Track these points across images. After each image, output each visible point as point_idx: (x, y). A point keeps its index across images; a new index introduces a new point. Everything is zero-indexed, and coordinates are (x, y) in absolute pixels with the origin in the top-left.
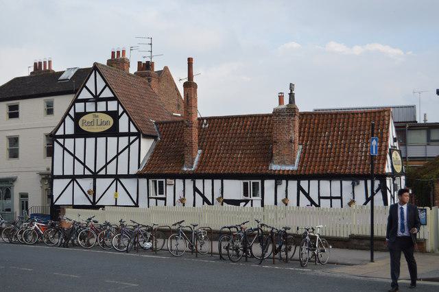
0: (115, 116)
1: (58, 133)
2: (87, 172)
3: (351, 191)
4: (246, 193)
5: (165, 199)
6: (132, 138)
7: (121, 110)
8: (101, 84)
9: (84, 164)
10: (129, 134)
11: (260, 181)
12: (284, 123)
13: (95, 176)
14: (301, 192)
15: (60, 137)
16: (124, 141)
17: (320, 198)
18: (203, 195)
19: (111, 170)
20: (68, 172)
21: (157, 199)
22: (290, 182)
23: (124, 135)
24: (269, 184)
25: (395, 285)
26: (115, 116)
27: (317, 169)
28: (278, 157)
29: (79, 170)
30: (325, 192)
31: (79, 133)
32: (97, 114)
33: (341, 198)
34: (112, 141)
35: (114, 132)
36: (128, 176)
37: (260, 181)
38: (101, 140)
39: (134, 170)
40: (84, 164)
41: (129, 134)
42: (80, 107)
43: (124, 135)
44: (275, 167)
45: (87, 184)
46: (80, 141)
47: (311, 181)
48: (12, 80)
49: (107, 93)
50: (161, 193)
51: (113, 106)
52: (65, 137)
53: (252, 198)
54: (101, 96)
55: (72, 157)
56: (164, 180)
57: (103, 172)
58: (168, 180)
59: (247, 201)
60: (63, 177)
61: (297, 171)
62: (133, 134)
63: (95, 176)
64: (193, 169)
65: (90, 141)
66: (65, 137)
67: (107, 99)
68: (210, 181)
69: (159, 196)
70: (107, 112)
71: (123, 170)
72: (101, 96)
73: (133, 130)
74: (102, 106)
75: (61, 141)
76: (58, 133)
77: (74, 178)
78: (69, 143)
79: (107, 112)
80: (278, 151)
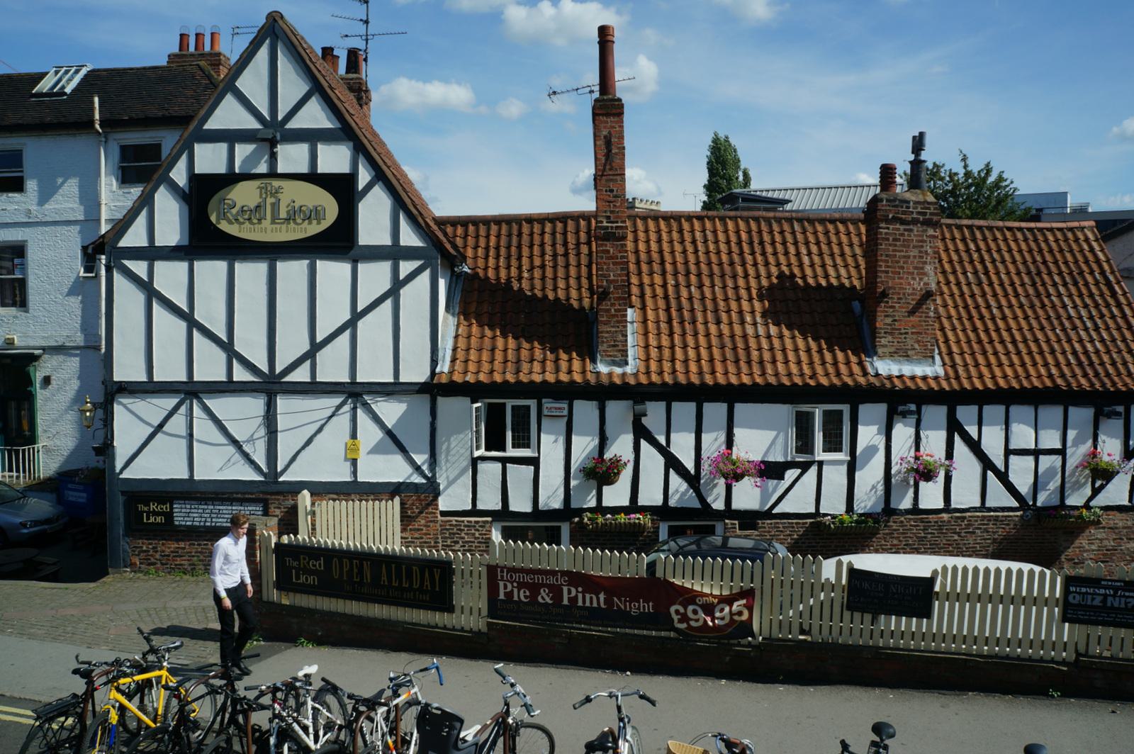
0: (343, 188)
1: (126, 241)
2: (240, 374)
3: (319, 436)
4: (805, 444)
5: (534, 462)
6: (406, 267)
7: (364, 176)
8: (292, 86)
9: (227, 347)
10: (394, 253)
11: (845, 408)
12: (906, 244)
13: (271, 386)
14: (957, 438)
15: (136, 253)
16: (376, 277)
17: (1008, 452)
18: (664, 451)
19: (332, 367)
20: (170, 369)
21: (504, 461)
22: (676, 406)
23: (375, 254)
24: (873, 413)
25: (244, 752)
26: (343, 188)
27: (1005, 377)
28: (890, 338)
29: (210, 366)
30: (1023, 436)
31: (205, 241)
32: (276, 183)
33: (1062, 452)
34: (333, 273)
35: (339, 241)
36: (392, 390)
37: (845, 408)
38: (292, 271)
39: (414, 371)
40: (227, 347)
41: (394, 253)
42: (210, 159)
43: (375, 254)
44: (885, 367)
45: (242, 413)
46: (211, 272)
47: (1072, 410)
48: (125, 70)
49: (315, 116)
50: (522, 442)
51: (335, 159)
52: (152, 253)
53: (820, 455)
54: (292, 125)
55: (183, 325)
56: (532, 403)
57: (301, 375)
58: (548, 404)
59: (805, 467)
60: (150, 388)
61: (636, 375)
62: (410, 253)
63: (271, 386)
64: (629, 369)
65: (251, 274)
66: (152, 253)
67: (312, 137)
68: (663, 405)
69: (511, 452)
70: (313, 177)
71: (375, 370)
72: (292, 125)
73: (409, 238)
74: (292, 157)
75: (139, 268)
76: (126, 241)
77: (191, 391)
78: (169, 278)
79: (313, 177)
80: (889, 320)
